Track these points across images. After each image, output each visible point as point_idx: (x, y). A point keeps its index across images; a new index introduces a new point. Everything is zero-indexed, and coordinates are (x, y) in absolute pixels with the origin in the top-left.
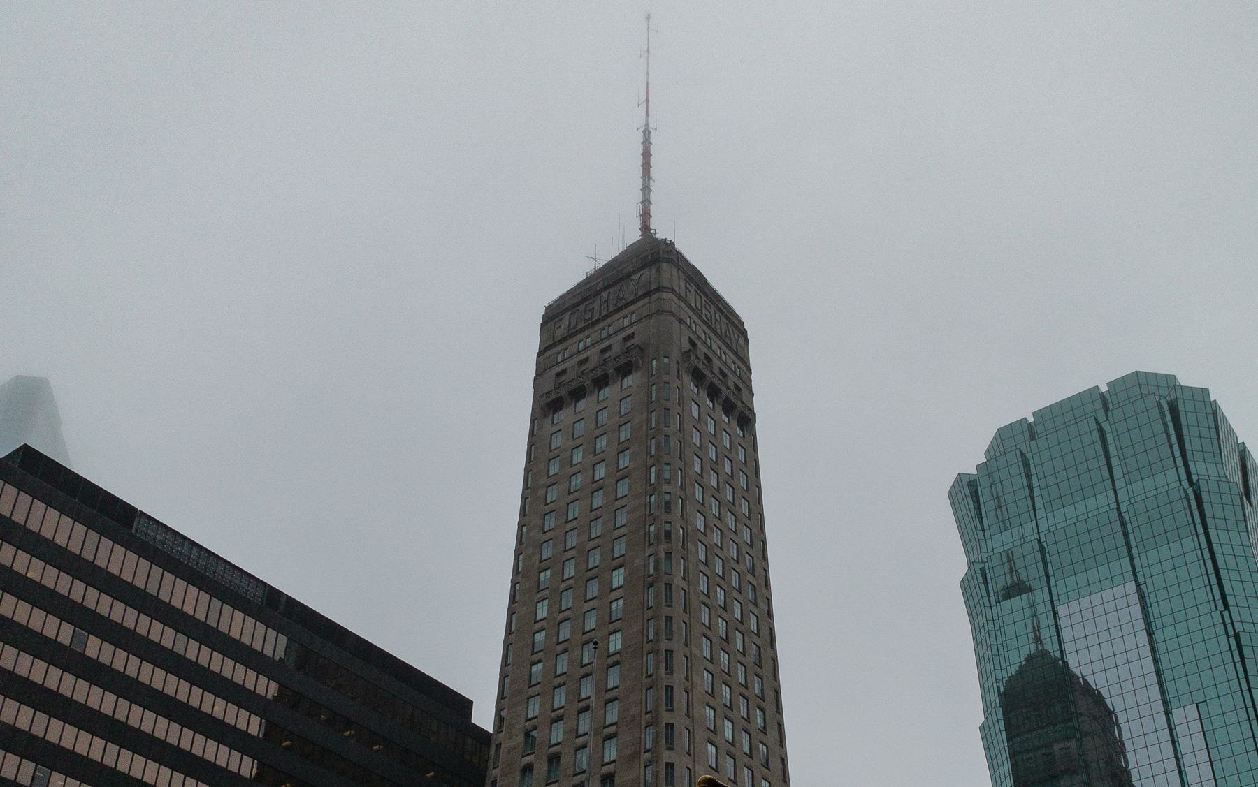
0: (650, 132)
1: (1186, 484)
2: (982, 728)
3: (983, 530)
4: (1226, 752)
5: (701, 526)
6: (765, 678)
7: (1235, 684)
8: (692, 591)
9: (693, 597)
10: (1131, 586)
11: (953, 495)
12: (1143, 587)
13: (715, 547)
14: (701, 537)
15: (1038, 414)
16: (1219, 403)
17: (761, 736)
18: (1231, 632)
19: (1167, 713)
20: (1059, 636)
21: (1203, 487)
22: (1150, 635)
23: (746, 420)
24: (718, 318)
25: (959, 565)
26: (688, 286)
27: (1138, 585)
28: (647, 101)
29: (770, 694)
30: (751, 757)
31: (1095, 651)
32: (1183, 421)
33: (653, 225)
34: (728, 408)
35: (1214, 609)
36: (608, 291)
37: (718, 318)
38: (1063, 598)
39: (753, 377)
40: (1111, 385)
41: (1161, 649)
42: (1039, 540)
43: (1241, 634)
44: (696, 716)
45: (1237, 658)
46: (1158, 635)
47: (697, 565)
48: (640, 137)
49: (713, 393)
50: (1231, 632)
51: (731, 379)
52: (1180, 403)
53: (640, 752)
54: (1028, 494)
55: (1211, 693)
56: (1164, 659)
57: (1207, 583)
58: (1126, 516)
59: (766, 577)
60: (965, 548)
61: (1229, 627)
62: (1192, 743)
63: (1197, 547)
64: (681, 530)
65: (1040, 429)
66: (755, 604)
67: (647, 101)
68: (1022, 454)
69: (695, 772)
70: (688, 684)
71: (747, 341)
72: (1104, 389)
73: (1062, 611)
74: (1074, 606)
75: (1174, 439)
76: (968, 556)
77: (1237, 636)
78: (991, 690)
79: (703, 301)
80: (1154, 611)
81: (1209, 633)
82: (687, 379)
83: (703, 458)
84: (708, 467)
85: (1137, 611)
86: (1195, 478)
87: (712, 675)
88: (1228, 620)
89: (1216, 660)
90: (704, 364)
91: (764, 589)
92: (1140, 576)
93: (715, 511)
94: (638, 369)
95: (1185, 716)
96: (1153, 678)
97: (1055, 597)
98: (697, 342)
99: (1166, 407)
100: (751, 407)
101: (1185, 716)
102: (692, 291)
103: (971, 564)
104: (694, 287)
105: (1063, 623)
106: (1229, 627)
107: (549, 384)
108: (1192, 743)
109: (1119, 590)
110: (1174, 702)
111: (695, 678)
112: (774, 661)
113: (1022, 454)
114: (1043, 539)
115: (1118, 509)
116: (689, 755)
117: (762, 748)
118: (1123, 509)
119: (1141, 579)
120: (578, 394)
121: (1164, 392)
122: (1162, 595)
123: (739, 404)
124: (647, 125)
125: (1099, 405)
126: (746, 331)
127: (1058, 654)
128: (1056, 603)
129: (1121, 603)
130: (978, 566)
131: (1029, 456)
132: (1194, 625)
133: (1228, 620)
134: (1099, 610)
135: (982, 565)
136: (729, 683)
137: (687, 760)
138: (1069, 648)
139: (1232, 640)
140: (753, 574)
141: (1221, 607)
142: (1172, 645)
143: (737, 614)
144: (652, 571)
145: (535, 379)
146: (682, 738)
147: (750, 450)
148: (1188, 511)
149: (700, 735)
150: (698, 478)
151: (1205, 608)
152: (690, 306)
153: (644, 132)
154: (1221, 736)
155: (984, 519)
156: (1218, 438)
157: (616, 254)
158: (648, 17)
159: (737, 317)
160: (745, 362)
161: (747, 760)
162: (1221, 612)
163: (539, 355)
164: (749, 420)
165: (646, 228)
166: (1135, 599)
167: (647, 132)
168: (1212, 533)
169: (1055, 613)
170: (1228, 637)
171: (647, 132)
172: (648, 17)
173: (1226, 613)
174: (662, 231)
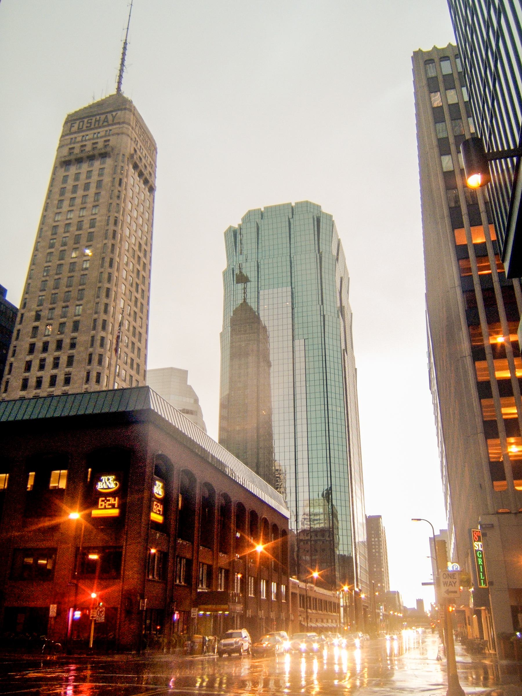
1: (317, 252)
3: (236, 252)
4: (311, 347)
5: (128, 235)
7: (322, 382)
10: (289, 288)
11: (226, 234)
12: (294, 289)
14: (128, 239)
15: (266, 208)
16: (335, 221)
18: (322, 314)
19: (293, 340)
20: (258, 303)
21: (323, 255)
25: (224, 265)
27: (292, 288)
28: (128, 28)
32: (321, 227)
33: (122, 88)
34: (146, 182)
36: (100, 116)
38: (263, 287)
39: (157, 169)
40: (297, 204)
42: (257, 262)
46: (296, 310)
49: (141, 174)
50: (322, 314)
51: (149, 168)
52: (321, 219)
54: (256, 241)
55: (310, 336)
56: (296, 320)
58: (292, 259)
60: (227, 257)
61: (322, 312)
62: (300, 354)
65: (265, 214)
67: (128, 28)
68: (257, 224)
71: (157, 153)
72: (293, 204)
73: (261, 292)
74: (266, 292)
75: (316, 233)
76: (228, 262)
77: (324, 316)
82: (131, 166)
83: (133, 203)
84: (134, 208)
88: (322, 309)
93: (134, 228)
94: (110, 157)
95: (299, 343)
97: (259, 286)
98: (137, 150)
99: (316, 219)
101: (299, 343)
103: (229, 265)
105: (261, 297)
106: (322, 312)
107: (65, 151)
108: (300, 354)
109: (284, 289)
110: (296, 337)
113: (257, 224)
114: (259, 261)
115: (290, 256)
118: (292, 256)
119: (293, 286)
120: (79, 161)
121: (316, 212)
124: (126, 40)
125: (290, 211)
127: (256, 310)
128: (259, 289)
130: (232, 267)
131: (260, 225)
133: (322, 309)
135: (233, 267)
138: (261, 308)
139: (322, 317)
141: (320, 303)
142: (300, 315)
147: (152, 203)
148: (316, 263)
151: (315, 303)
152: (136, 133)
154: (312, 377)
155: (340, 530)
157: (104, 98)
163: (62, 136)
165: (119, 89)
166: (290, 294)
167: (125, 43)
168: (323, 273)
169: (258, 293)
170: (321, 315)
171: (125, 43)
173: (322, 306)
174: (127, 93)
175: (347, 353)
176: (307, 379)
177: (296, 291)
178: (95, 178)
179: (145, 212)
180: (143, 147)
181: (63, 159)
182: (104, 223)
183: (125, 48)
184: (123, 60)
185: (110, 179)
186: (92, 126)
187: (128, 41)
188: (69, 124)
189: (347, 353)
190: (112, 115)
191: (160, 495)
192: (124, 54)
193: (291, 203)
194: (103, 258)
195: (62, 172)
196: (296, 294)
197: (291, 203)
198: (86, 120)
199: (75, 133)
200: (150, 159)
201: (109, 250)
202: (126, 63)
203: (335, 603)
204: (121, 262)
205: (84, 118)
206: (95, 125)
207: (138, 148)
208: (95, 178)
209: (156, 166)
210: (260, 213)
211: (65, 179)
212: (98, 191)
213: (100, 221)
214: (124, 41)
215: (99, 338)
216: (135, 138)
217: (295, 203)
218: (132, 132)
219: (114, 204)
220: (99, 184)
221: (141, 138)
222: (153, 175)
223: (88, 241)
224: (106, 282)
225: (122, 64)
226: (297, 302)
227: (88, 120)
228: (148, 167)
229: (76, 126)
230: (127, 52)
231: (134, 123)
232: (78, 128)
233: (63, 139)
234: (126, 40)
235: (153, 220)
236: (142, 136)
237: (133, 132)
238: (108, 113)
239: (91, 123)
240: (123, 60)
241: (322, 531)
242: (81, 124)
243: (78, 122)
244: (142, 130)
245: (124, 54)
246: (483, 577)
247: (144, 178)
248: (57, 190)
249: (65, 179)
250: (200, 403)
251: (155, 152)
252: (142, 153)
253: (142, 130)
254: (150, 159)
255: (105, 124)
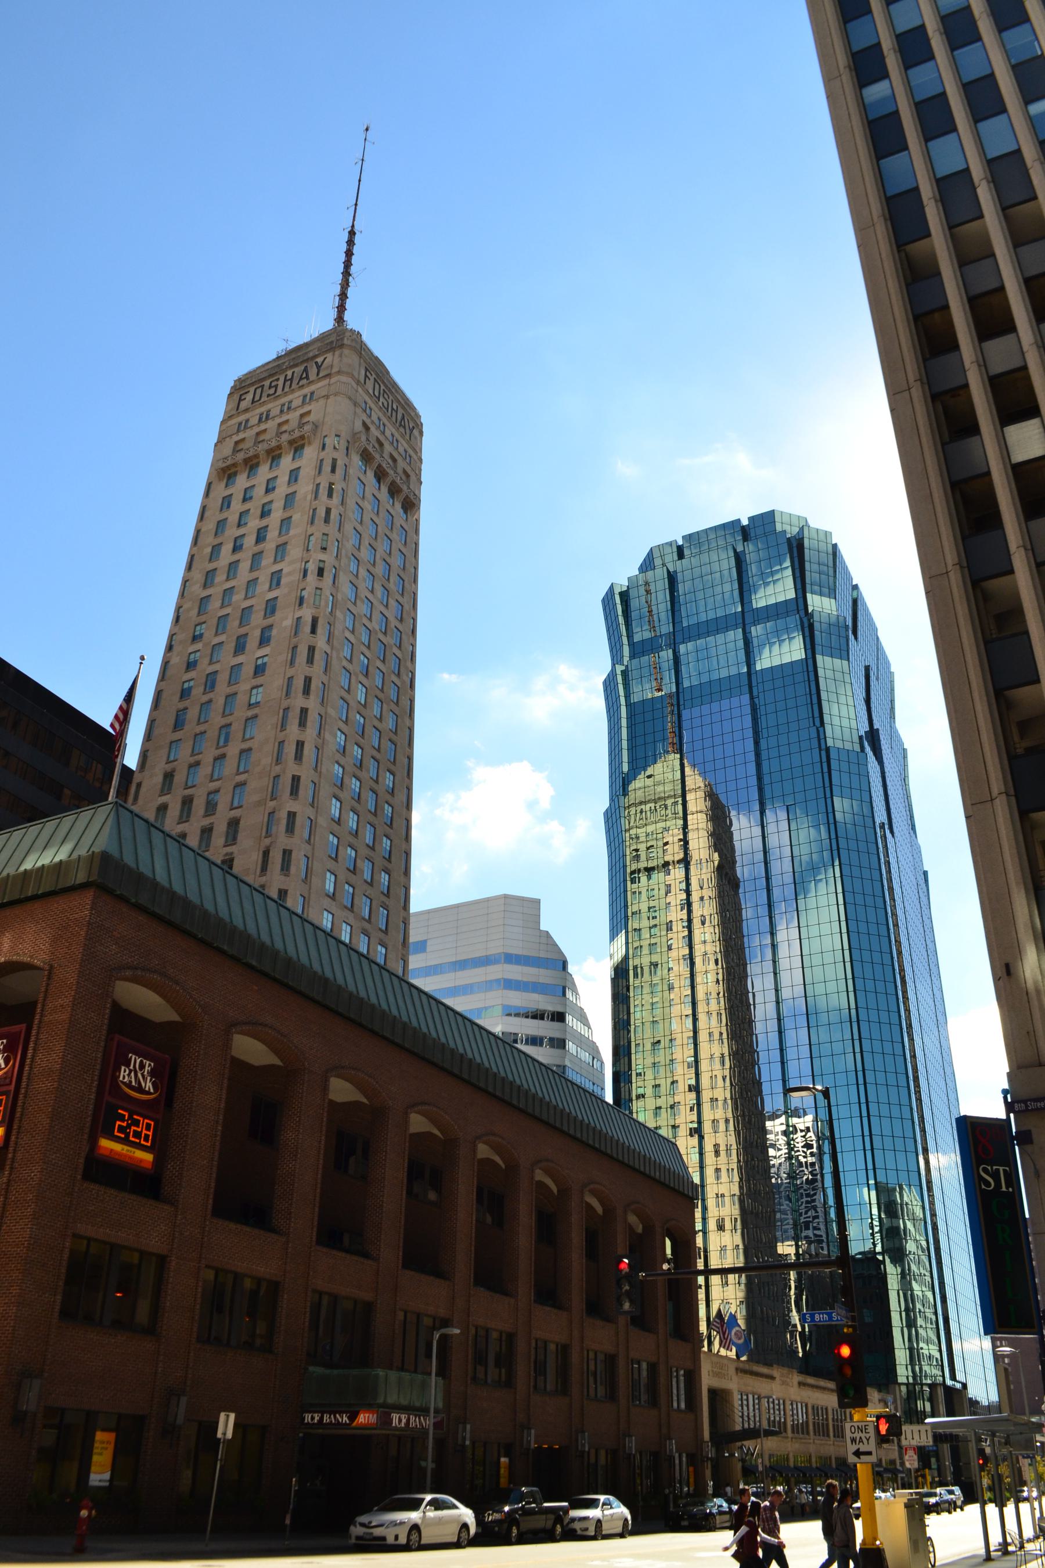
0: (354, 234)
1: (802, 613)
2: (606, 813)
6: (399, 744)
8: (334, 655)
9: (334, 662)
10: (746, 699)
12: (756, 700)
13: (375, 719)
17: (388, 797)
22: (757, 743)
23: (411, 505)
24: (395, 407)
26: (368, 373)
27: (752, 698)
29: (402, 760)
30: (375, 814)
31: (719, 750)
34: (394, 491)
35: (812, 725)
37: (395, 407)
38: (688, 704)
40: (752, 519)
41: (764, 755)
43: (831, 749)
44: (324, 770)
45: (825, 770)
47: (343, 632)
48: (345, 237)
50: (823, 746)
51: (401, 464)
53: (266, 799)
57: (809, 702)
59: (412, 652)
63: (805, 669)
64: (331, 598)
66: (399, 675)
67: (356, 205)
69: (316, 823)
70: (321, 741)
71: (421, 433)
73: (686, 714)
74: (696, 711)
78: (617, 780)
79: (382, 391)
80: (763, 723)
81: (805, 745)
85: (748, 721)
86: (810, 610)
87: (346, 735)
89: (808, 770)
90: (374, 447)
91: (409, 664)
92: (755, 690)
96: (753, 781)
98: (370, 425)
100: (416, 493)
102: (372, 380)
104: (374, 376)
107: (228, 449)
109: (735, 701)
111: (327, 736)
112: (411, 730)
116: (313, 807)
117: (388, 810)
119: (755, 693)
122: (771, 708)
123: (405, 488)
124: (353, 226)
126: (422, 424)
128: (682, 707)
129: (736, 712)
132: (794, 737)
134: (726, 715)
136: (361, 745)
137: (310, 812)
139: (824, 753)
140: (400, 647)
141: (818, 723)
142: (774, 753)
143: (379, 683)
144: (806, 1325)
145: (216, 445)
146: (306, 790)
149: (325, 790)
150: (377, 723)
151: (804, 724)
153: (350, 232)
156: (835, 576)
158: (367, 129)
159: (414, 409)
160: (417, 450)
161: (371, 818)
162: (817, 728)
163: (222, 423)
164: (414, 504)
165: (340, 319)
166: (748, 710)
167: (352, 233)
171: (352, 233)
172: (367, 129)
173: (821, 729)
175: (892, 832)
176: (805, 952)
177: (762, 703)
178: (282, 489)
179: (395, 551)
180: (384, 420)
181: (222, 465)
182: (297, 576)
183: (351, 242)
184: (348, 264)
185: (311, 487)
186: (279, 391)
187: (357, 229)
188: (236, 397)
189: (892, 832)
190: (316, 363)
191: (150, 1094)
192: (349, 254)
193: (739, 521)
194: (295, 648)
195: (220, 491)
196: (762, 708)
197: (739, 521)
198: (267, 383)
199: (247, 410)
200: (403, 445)
201: (308, 629)
202: (353, 270)
203: (798, 1432)
204: (334, 653)
205: (264, 379)
206: (283, 390)
207: (373, 422)
208: (282, 489)
209: (421, 460)
210: (675, 549)
211: (227, 501)
212: (287, 515)
213: (289, 574)
214: (350, 229)
215: (283, 815)
216: (366, 403)
217: (749, 518)
218: (357, 391)
219: (318, 535)
220: (290, 499)
221: (380, 404)
222: (413, 478)
223: (265, 617)
224: (300, 695)
225: (346, 273)
226: (764, 725)
227: (271, 383)
228: (400, 460)
229: (249, 397)
230: (356, 250)
231: (363, 372)
232: (253, 402)
233: (224, 427)
234: (353, 226)
235: (416, 568)
236: (381, 399)
237: (360, 390)
238: (307, 360)
239: (276, 386)
240: (348, 264)
241: (869, 1252)
242: (259, 391)
243: (252, 390)
244: (382, 387)
245: (349, 254)
246: (1007, 1188)
247: (402, 496)
248: (210, 526)
249: (227, 501)
250: (571, 969)
251: (416, 432)
252: (383, 433)
253: (382, 387)
254: (403, 445)
255: (304, 381)
